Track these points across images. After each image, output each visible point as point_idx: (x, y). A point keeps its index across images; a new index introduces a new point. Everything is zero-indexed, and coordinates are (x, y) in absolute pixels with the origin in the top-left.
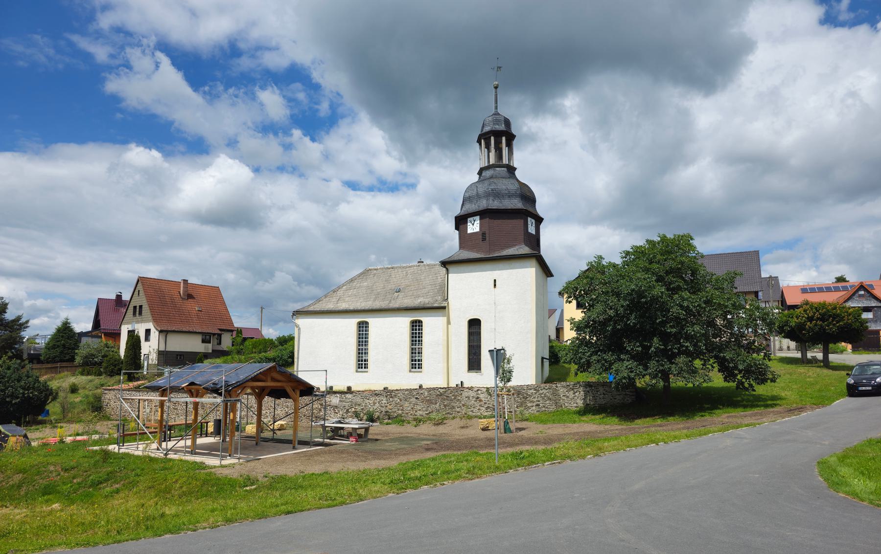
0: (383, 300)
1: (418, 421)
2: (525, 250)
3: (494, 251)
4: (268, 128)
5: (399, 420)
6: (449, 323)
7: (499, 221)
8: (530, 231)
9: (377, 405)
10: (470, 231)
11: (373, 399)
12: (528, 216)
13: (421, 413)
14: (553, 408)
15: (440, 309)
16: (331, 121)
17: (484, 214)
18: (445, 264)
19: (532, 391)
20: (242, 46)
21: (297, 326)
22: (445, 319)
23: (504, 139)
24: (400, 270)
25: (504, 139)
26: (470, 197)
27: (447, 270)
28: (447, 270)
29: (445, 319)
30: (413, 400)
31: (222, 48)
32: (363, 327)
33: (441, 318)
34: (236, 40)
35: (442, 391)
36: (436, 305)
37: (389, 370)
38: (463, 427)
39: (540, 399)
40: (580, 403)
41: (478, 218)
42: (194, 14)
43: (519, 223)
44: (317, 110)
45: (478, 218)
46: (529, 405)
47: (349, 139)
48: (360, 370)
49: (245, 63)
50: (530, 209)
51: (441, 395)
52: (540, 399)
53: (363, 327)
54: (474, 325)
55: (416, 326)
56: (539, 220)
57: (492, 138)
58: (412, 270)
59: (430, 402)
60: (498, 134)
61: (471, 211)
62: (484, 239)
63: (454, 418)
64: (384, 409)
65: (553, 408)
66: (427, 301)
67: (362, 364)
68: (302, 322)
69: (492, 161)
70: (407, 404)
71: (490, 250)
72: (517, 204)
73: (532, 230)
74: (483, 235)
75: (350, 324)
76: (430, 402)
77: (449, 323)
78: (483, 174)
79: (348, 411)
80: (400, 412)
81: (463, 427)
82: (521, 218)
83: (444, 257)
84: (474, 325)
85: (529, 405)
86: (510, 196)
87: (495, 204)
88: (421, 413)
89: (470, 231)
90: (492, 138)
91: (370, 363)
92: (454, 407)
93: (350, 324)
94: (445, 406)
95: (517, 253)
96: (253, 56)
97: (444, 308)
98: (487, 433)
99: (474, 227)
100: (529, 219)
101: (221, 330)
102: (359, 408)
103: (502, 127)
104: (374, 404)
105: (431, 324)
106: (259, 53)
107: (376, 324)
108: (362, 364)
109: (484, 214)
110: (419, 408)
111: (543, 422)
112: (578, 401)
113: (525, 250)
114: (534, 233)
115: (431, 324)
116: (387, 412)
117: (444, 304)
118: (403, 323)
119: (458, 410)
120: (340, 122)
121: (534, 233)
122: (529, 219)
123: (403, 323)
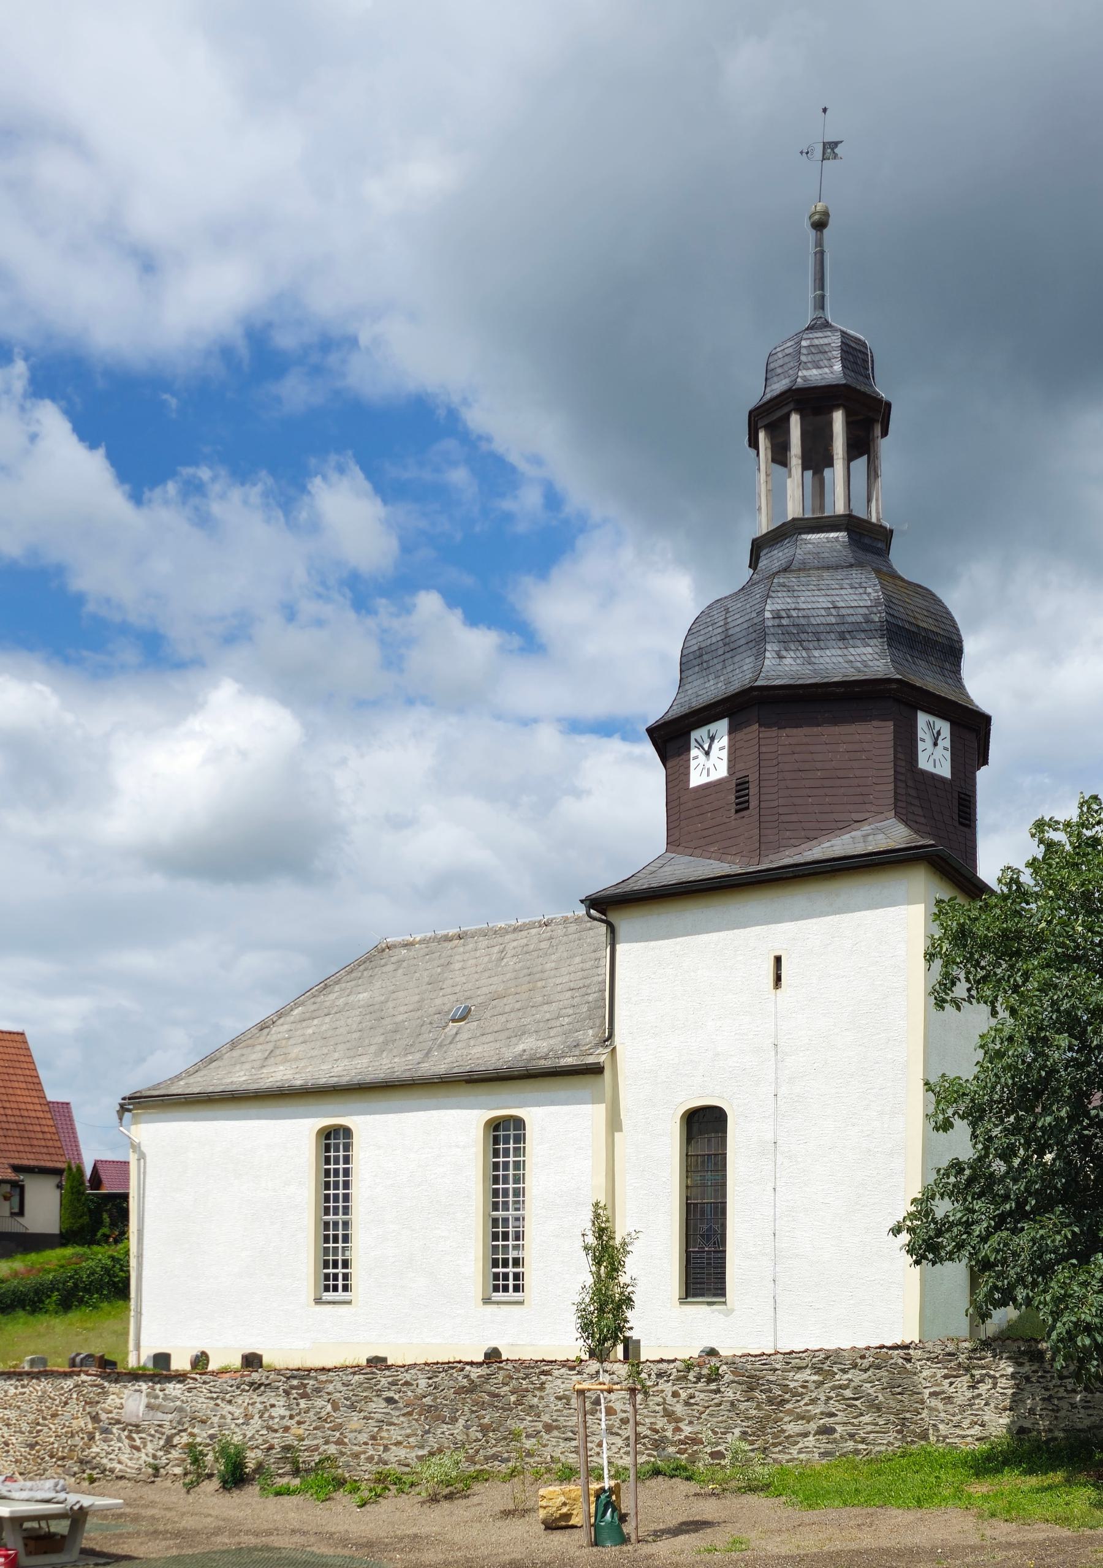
0: (407, 1050)
1: (386, 1482)
2: (891, 833)
3: (778, 848)
4: (361, 592)
5: (324, 1478)
6: (614, 1123)
7: (799, 735)
8: (924, 763)
9: (256, 1422)
10: (697, 779)
11: (243, 1399)
12: (915, 708)
13: (402, 1453)
14: (887, 1442)
15: (583, 1074)
16: (551, 545)
17: (747, 708)
18: (609, 906)
19: (806, 1375)
20: (285, 340)
21: (136, 1147)
22: (597, 1112)
23: (838, 419)
24: (483, 942)
25: (838, 419)
26: (701, 652)
27: (612, 929)
28: (612, 929)
29: (597, 1112)
30: (378, 1406)
31: (226, 353)
32: (334, 1142)
33: (587, 1109)
34: (270, 325)
35: (475, 1373)
36: (569, 1061)
37: (423, 1304)
38: (507, 1514)
39: (834, 1406)
40: (998, 1424)
41: (722, 726)
42: (147, 263)
43: (874, 736)
44: (508, 517)
45: (722, 726)
46: (792, 1428)
47: (609, 595)
48: (330, 1296)
49: (295, 393)
50: (930, 681)
51: (472, 1388)
52: (834, 1406)
53: (334, 1142)
54: (705, 1127)
55: (505, 1134)
56: (972, 730)
57: (795, 420)
58: (522, 939)
59: (433, 1414)
60: (813, 402)
61: (698, 702)
62: (742, 806)
63: (513, 1473)
64: (276, 1440)
65: (887, 1442)
66: (543, 1046)
67: (334, 1276)
68: (153, 1134)
69: (793, 509)
70: (355, 1421)
71: (762, 847)
72: (869, 659)
73: (935, 757)
74: (739, 789)
75: (295, 1135)
76: (433, 1414)
77: (614, 1123)
78: (763, 563)
79: (169, 1445)
80: (332, 1449)
81: (507, 1514)
82: (883, 718)
83: (604, 881)
84: (705, 1127)
85: (792, 1428)
86: (846, 632)
87: (783, 666)
88: (402, 1453)
89: (697, 779)
90: (795, 420)
91: (357, 1272)
92: (515, 1436)
93: (295, 1135)
94: (485, 1429)
95: (860, 849)
96: (317, 371)
97: (596, 1070)
98: (559, 1539)
99: (710, 762)
100: (922, 719)
101: (17, 1169)
102: (202, 1435)
103: (832, 371)
104: (248, 1417)
105: (556, 1129)
106: (333, 359)
107: (374, 1131)
108: (334, 1276)
109: (747, 708)
110: (396, 1434)
111: (847, 1497)
112: (989, 1415)
113: (891, 833)
114: (944, 770)
115: (556, 1129)
116: (287, 1448)
117: (601, 1056)
118: (462, 1125)
119: (529, 1444)
120: (580, 542)
121: (944, 770)
122: (922, 719)
123: (462, 1125)
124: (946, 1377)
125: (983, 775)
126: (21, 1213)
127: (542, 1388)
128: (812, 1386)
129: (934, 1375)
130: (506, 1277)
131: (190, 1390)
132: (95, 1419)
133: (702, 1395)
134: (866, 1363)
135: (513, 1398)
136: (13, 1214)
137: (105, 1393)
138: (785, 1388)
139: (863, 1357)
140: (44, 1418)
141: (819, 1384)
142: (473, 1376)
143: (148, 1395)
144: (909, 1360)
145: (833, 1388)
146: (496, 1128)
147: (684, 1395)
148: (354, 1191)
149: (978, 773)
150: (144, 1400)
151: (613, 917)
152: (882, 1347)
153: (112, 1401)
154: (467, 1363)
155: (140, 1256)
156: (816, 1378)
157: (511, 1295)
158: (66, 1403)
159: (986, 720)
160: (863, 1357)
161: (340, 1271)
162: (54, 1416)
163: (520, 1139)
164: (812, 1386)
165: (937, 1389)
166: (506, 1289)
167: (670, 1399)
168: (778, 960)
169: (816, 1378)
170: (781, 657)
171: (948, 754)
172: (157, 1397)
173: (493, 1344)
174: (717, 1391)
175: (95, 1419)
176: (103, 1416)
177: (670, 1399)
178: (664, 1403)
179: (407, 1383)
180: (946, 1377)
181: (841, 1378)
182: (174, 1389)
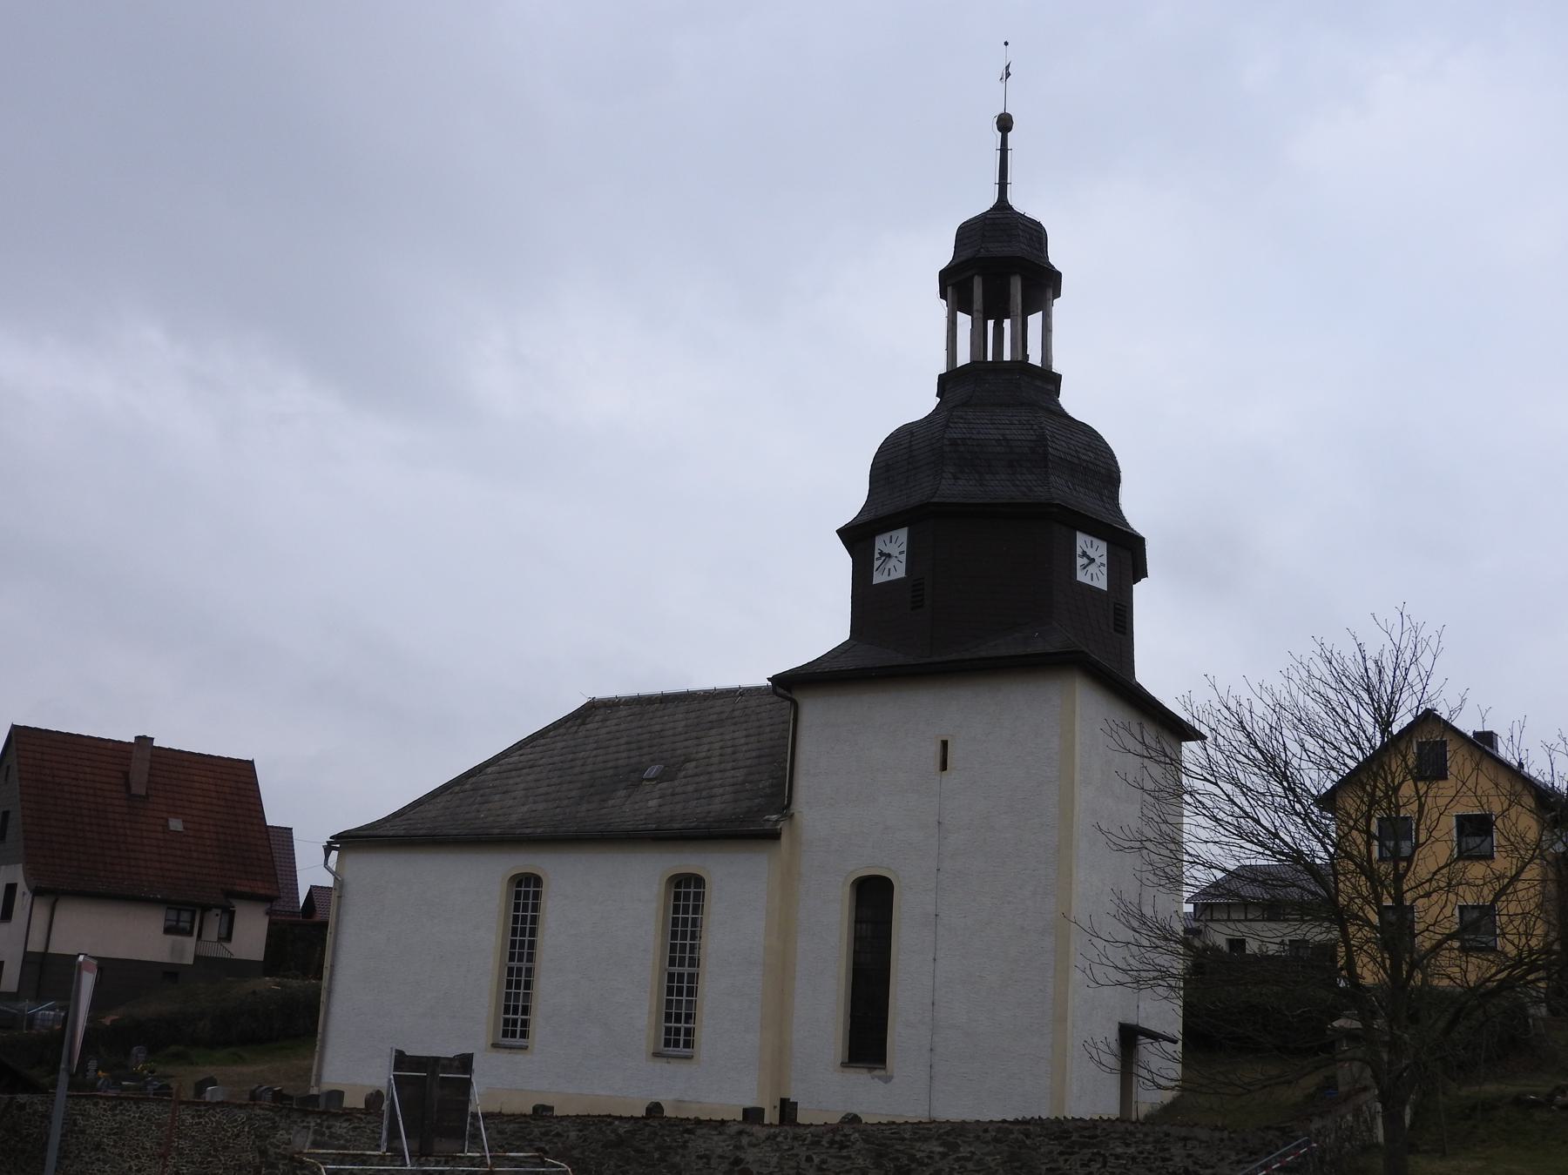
10: (878, 578)
28: (796, 706)
50: (1086, 502)
53: (526, 891)
54: (873, 899)
84: (873, 899)
89: (878, 578)
114: (1101, 583)
121: (1101, 583)
124: (1061, 1153)
125: (1139, 589)
126: (228, 938)
127: (684, 1146)
128: (937, 1158)
129: (1051, 1152)
130: (678, 1031)
131: (355, 1129)
132: (263, 1153)
133: (834, 1161)
134: (988, 1137)
135: (656, 1155)
136: (220, 939)
137: (275, 1128)
138: (912, 1158)
139: (986, 1131)
140: (216, 1150)
141: (944, 1156)
142: (621, 1131)
143: (315, 1132)
144: (1027, 1136)
145: (958, 1160)
146: (678, 885)
147: (816, 1160)
148: (539, 939)
149: (1136, 587)
150: (311, 1137)
151: (797, 696)
152: (1004, 1121)
153: (282, 1135)
154: (616, 1118)
155: (330, 992)
156: (941, 1149)
157: (682, 1050)
158: (238, 1136)
159: (1141, 541)
160: (986, 1131)
161: (520, 1017)
162: (226, 1148)
163: (699, 897)
164: (937, 1158)
165: (1053, 1165)
166: (677, 1044)
167: (804, 1165)
168: (945, 744)
169: (941, 1149)
170: (956, 478)
171: (1104, 570)
172: (323, 1134)
173: (655, 1099)
174: (848, 1158)
175: (263, 1153)
176: (272, 1151)
177: (804, 1165)
178: (798, 1167)
179: (558, 1135)
180: (1061, 1153)
181: (964, 1151)
182: (341, 1127)
